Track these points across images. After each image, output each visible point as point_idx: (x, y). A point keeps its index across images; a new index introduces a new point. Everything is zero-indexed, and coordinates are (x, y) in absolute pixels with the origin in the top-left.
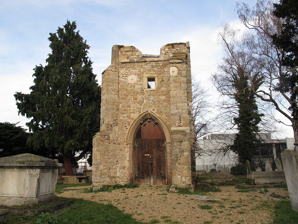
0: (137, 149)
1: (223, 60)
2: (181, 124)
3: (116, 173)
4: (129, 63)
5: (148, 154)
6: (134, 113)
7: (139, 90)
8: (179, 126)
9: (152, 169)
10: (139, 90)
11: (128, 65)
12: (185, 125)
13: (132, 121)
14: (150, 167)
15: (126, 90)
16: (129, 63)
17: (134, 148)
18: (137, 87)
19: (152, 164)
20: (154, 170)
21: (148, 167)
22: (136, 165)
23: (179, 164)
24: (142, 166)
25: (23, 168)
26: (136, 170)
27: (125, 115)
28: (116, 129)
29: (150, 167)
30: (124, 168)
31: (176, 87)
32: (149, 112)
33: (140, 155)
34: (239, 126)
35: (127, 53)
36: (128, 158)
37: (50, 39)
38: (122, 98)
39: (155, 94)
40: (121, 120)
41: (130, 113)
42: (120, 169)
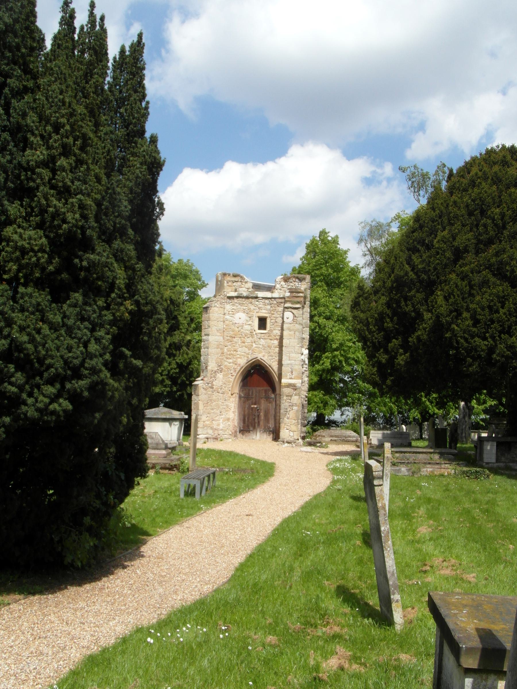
0: (243, 399)
1: (334, 600)
2: (293, 376)
3: (218, 425)
4: (237, 297)
5: (255, 404)
6: (240, 358)
7: (248, 332)
8: (291, 378)
9: (259, 422)
10: (248, 332)
11: (236, 300)
12: (297, 378)
13: (239, 368)
14: (256, 419)
15: (233, 331)
16: (237, 297)
17: (240, 397)
18: (247, 327)
19: (259, 416)
20: (262, 423)
21: (254, 419)
22: (242, 417)
23: (288, 418)
24: (248, 418)
25: (442, 656)
26: (242, 424)
27: (231, 361)
28: (220, 376)
29: (256, 419)
30: (228, 419)
31: (290, 335)
32: (259, 358)
33: (247, 406)
34: (348, 266)
35: (234, 284)
36: (232, 410)
37: (338, 596)
38: (228, 340)
39: (266, 337)
40: (226, 366)
41: (237, 358)
42: (224, 421)
